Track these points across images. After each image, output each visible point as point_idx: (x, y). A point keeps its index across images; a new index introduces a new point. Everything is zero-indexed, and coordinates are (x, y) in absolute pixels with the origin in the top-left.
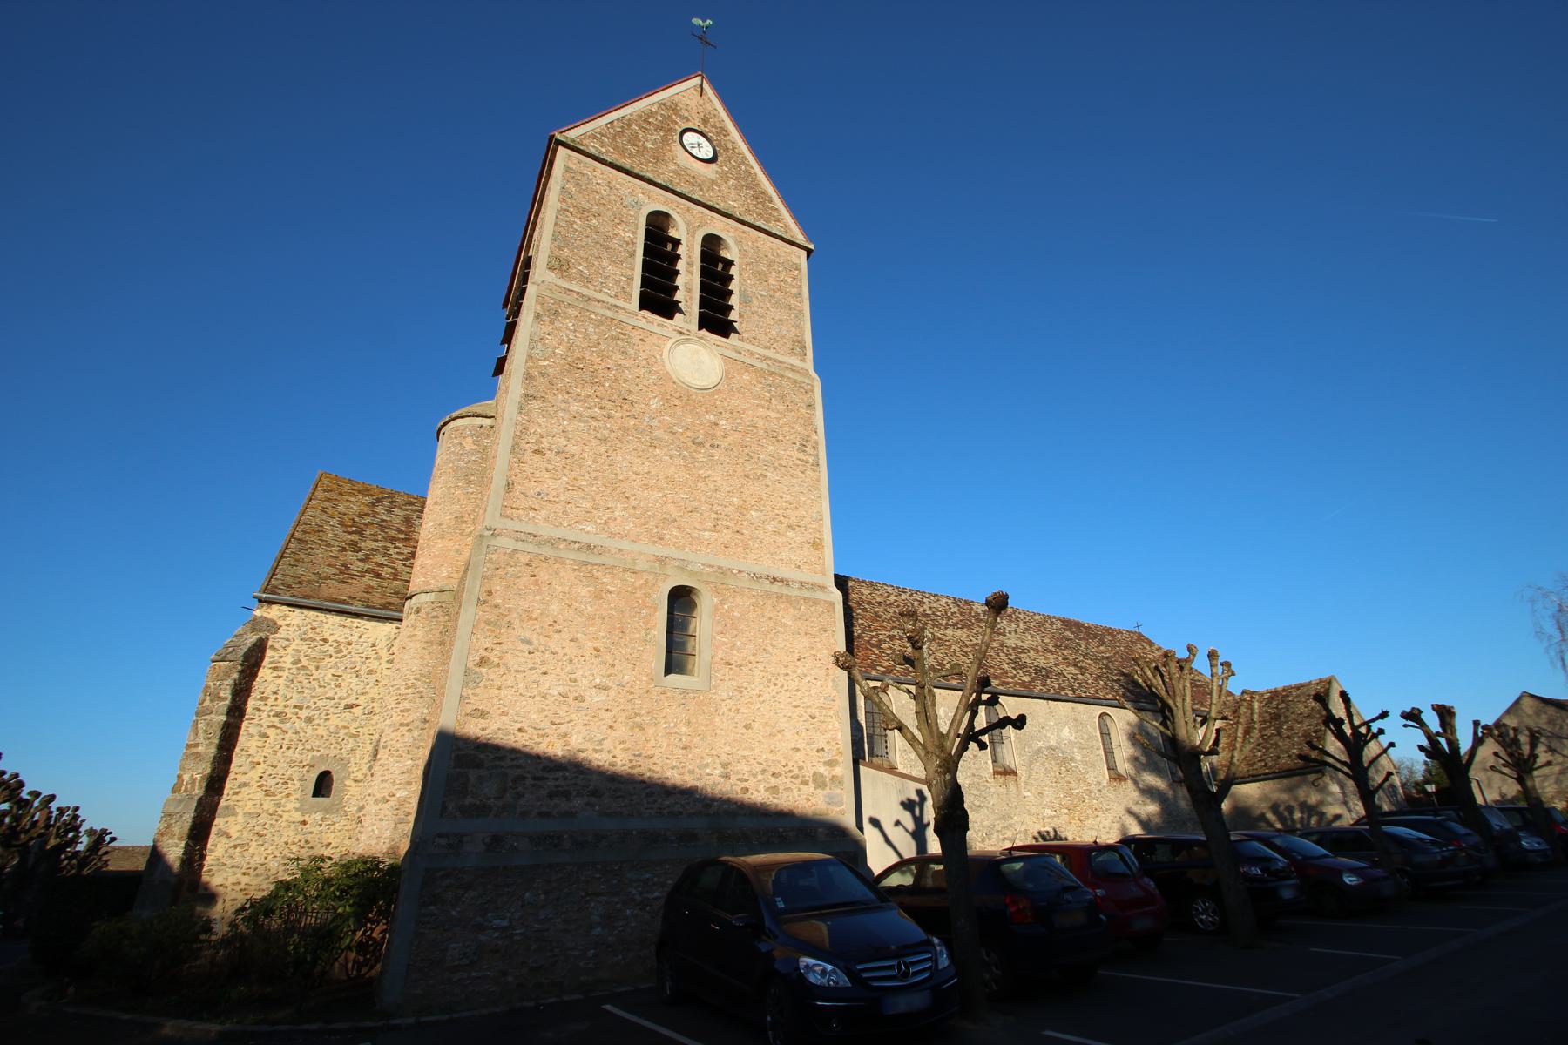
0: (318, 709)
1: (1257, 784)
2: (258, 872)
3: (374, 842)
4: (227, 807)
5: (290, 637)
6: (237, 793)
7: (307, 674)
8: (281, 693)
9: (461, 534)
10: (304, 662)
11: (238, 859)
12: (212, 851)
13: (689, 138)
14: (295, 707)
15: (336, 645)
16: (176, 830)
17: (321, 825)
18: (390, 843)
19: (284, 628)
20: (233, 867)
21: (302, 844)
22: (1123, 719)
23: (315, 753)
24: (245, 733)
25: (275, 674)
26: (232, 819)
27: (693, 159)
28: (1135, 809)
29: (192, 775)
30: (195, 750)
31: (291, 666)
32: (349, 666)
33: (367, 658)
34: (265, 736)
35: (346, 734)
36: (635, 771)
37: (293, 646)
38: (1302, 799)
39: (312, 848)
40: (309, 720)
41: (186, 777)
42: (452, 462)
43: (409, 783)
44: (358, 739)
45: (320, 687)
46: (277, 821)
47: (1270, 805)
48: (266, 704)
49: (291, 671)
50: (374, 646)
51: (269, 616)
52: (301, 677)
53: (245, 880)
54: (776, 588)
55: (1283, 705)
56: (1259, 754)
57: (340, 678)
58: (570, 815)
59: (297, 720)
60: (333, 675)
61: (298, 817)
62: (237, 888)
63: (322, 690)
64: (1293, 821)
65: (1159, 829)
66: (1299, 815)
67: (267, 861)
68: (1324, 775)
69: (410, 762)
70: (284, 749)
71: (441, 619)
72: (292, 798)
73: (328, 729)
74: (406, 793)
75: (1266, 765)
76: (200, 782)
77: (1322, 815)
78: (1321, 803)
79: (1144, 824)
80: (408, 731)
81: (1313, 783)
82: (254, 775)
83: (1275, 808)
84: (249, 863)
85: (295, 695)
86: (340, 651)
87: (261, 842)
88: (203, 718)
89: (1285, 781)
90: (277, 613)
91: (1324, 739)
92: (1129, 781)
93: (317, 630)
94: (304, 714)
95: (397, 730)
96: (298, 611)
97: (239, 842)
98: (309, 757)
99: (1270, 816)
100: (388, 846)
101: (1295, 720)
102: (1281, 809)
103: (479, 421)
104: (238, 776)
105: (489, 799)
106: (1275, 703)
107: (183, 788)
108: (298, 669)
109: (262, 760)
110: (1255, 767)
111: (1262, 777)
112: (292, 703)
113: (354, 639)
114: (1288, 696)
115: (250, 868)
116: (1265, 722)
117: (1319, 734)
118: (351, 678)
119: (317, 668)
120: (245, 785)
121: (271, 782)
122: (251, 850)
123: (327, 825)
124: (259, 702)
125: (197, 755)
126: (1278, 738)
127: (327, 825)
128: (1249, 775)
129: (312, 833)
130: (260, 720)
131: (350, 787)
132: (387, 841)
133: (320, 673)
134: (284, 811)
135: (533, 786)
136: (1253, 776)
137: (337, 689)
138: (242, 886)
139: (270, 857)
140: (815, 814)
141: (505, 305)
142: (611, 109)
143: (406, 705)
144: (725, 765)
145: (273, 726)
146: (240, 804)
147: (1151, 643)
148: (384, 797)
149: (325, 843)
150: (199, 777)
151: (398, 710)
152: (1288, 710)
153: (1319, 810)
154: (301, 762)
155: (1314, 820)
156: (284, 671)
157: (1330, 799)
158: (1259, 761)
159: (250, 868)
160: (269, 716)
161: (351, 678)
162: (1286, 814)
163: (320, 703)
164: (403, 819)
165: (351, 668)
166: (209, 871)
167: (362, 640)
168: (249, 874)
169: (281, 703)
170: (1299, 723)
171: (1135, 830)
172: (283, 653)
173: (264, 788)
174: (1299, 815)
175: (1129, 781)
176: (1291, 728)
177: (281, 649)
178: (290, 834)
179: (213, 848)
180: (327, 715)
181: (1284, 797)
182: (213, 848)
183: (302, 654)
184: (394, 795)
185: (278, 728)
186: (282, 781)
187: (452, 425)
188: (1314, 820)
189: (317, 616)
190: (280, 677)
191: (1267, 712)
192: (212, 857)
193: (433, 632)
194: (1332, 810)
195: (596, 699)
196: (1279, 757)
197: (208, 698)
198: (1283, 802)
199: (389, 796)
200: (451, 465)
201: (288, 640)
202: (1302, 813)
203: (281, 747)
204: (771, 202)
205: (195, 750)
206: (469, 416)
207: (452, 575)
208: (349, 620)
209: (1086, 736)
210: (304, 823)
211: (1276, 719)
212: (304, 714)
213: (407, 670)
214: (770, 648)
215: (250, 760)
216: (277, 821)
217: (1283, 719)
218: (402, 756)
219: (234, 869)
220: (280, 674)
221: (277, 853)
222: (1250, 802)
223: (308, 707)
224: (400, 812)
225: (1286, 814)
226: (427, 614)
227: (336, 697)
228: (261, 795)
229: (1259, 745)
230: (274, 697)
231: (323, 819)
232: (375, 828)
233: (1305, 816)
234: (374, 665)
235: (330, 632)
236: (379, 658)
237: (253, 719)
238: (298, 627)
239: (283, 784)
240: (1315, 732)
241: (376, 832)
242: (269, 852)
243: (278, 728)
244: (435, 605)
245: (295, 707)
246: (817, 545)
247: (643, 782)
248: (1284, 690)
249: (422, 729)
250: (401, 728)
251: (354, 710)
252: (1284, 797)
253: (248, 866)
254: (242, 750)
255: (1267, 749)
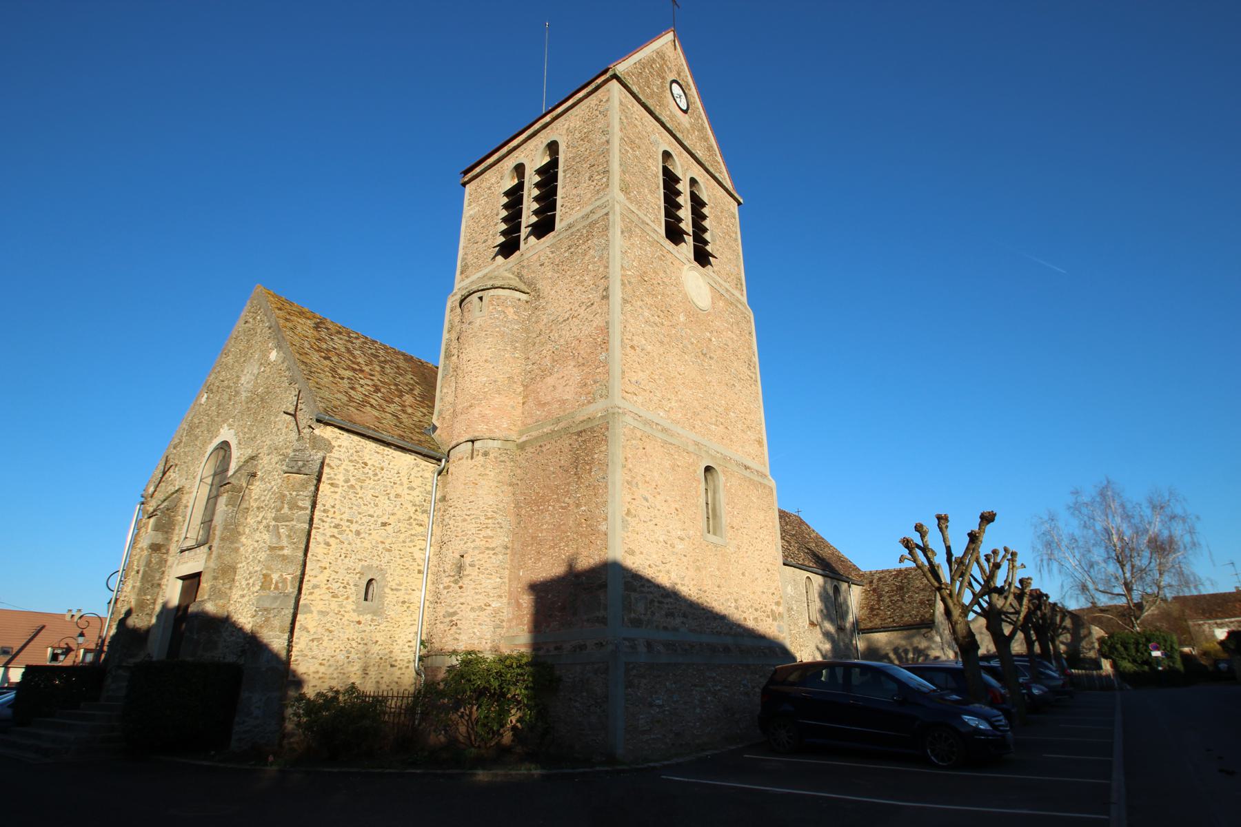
0: (362, 524)
1: (886, 633)
2: (330, 663)
3: (476, 642)
4: (305, 605)
5: (342, 458)
6: (311, 593)
7: (355, 492)
8: (337, 507)
9: (514, 392)
10: (353, 482)
11: (316, 652)
12: (297, 643)
13: (675, 86)
14: (348, 521)
15: (373, 469)
16: (276, 623)
17: (370, 625)
18: (491, 643)
19: (337, 448)
20: (313, 658)
21: (359, 641)
22: (818, 580)
23: (363, 563)
24: (314, 540)
25: (333, 489)
26: (309, 616)
27: (677, 108)
28: (820, 646)
29: (282, 575)
30: (281, 553)
31: (343, 484)
32: (382, 488)
33: (395, 483)
34: (328, 544)
35: (383, 548)
36: (700, 601)
37: (343, 466)
38: (915, 645)
39: (366, 644)
40: (358, 533)
41: (275, 577)
42: (497, 326)
43: (500, 597)
44: (391, 553)
45: (364, 505)
46: (341, 619)
47: (893, 647)
48: (328, 516)
49: (344, 489)
50: (398, 473)
51: (326, 436)
52: (352, 496)
53: (322, 669)
54: (747, 473)
55: (906, 581)
56: (889, 613)
57: (377, 499)
58: (676, 629)
59: (350, 532)
60: (373, 496)
61: (355, 617)
62: (317, 676)
63: (365, 508)
64: (907, 660)
65: (830, 658)
66: (912, 656)
67: (336, 654)
68: (932, 630)
69: (498, 580)
70: (343, 557)
71: (508, 463)
72: (350, 600)
73: (371, 543)
74: (500, 604)
75: (894, 621)
76: (292, 582)
77: (927, 656)
78: (928, 648)
79: (824, 656)
80: (494, 554)
81: (924, 636)
82: (322, 578)
83: (896, 650)
84: (323, 655)
85: (347, 510)
86: (376, 475)
87: (331, 638)
88: (283, 523)
89: (905, 632)
90: (331, 434)
91: (934, 606)
92: (818, 627)
93: (360, 454)
94: (354, 527)
95: (483, 553)
96: (346, 434)
97: (315, 636)
98: (360, 566)
99: (892, 655)
100: (490, 645)
101: (914, 591)
102: (900, 651)
103: (518, 294)
104: (311, 578)
105: (641, 615)
106: (900, 578)
107: (273, 586)
108: (348, 487)
109: (328, 565)
110: (886, 621)
111: (882, 629)
112: (345, 517)
113: (385, 465)
114: (909, 574)
115: (324, 659)
116: (893, 591)
117: (930, 602)
118: (384, 499)
119: (361, 488)
120: (315, 587)
121: (335, 586)
122: (325, 644)
123: (374, 626)
124: (323, 514)
125: (284, 558)
126: (903, 603)
127: (374, 626)
128: (882, 627)
129: (365, 631)
130: (324, 530)
131: (388, 594)
132: (489, 641)
133: (364, 493)
134: (346, 612)
135: (658, 607)
136: (884, 628)
137: (376, 508)
138: (320, 675)
139: (338, 651)
140: (774, 638)
141: (674, 234)
142: (638, 49)
143: (489, 532)
144: (736, 601)
145: (334, 536)
146: (313, 603)
147: (809, 527)
148: (480, 606)
149: (374, 641)
150: (289, 577)
151: (481, 536)
152: (909, 584)
153: (925, 653)
154: (354, 570)
155: (921, 659)
156: (338, 487)
157: (933, 646)
158: (890, 618)
159: (324, 659)
160: (330, 527)
161: (384, 499)
162: (903, 654)
163: (364, 519)
164: (500, 625)
165: (384, 491)
166: (296, 660)
167: (390, 466)
168: (324, 665)
169: (338, 516)
170: (917, 593)
171: (819, 658)
172: (336, 472)
173: (331, 591)
174: (912, 656)
175: (818, 627)
176: (911, 597)
177: (335, 468)
178: (351, 632)
179: (297, 641)
180: (370, 530)
181: (903, 642)
182: (297, 641)
183: (350, 473)
184: (489, 605)
185: (337, 538)
186: (343, 585)
187: (492, 292)
188: (921, 659)
189: (360, 441)
190: (336, 493)
191: (894, 584)
192: (297, 649)
193: (504, 474)
194: (935, 653)
195: (680, 547)
196: (903, 616)
197: (286, 506)
198: (903, 646)
199: (485, 605)
200: (498, 329)
201: (340, 460)
202: (914, 654)
203: (340, 556)
204: (716, 155)
205: (281, 553)
206: (510, 289)
207: (511, 427)
208: (382, 447)
209: (799, 593)
210: (359, 623)
211: (901, 590)
212: (354, 527)
213: (484, 503)
214: (748, 518)
215: (319, 565)
216: (341, 619)
217: (905, 590)
218: (492, 575)
219: (314, 660)
220: (336, 490)
221: (342, 648)
222: (879, 644)
223: (357, 522)
224: (496, 619)
225: (903, 654)
226: (496, 458)
227: (375, 515)
228: (328, 596)
229: (889, 606)
230: (332, 510)
231: (372, 620)
232: (476, 630)
233: (916, 657)
234: (399, 491)
235: (368, 457)
236: (402, 484)
237: (319, 528)
238: (347, 449)
239: (343, 587)
240: (928, 601)
241: (478, 634)
242: (337, 646)
243: (337, 538)
244: (501, 451)
245: (348, 521)
246: (760, 442)
247: (703, 609)
248: (906, 570)
249: (504, 554)
250: (487, 552)
251: (387, 528)
252: (903, 642)
253: (324, 658)
254: (313, 555)
255: (895, 610)
